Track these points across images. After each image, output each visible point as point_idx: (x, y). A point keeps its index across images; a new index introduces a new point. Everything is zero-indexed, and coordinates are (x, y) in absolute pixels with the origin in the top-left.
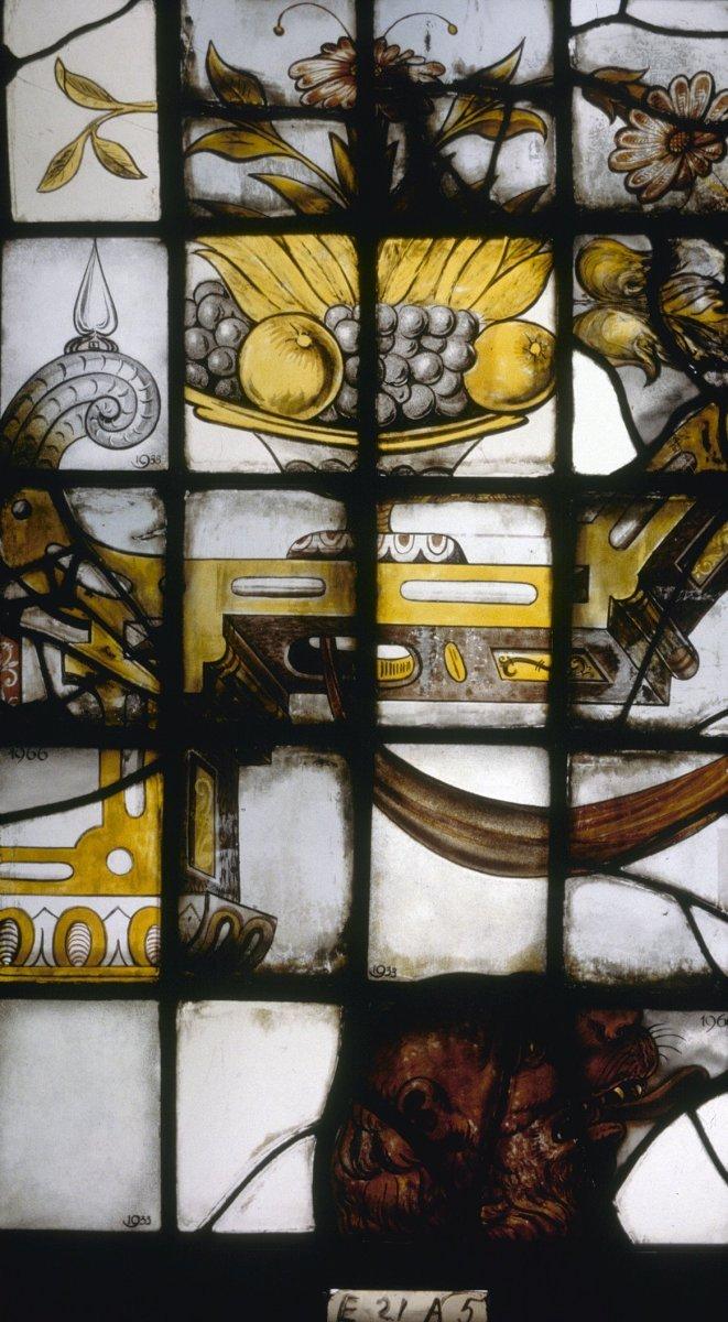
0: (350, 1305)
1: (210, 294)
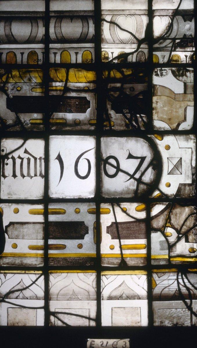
0: (93, 343)
1: (89, 51)
